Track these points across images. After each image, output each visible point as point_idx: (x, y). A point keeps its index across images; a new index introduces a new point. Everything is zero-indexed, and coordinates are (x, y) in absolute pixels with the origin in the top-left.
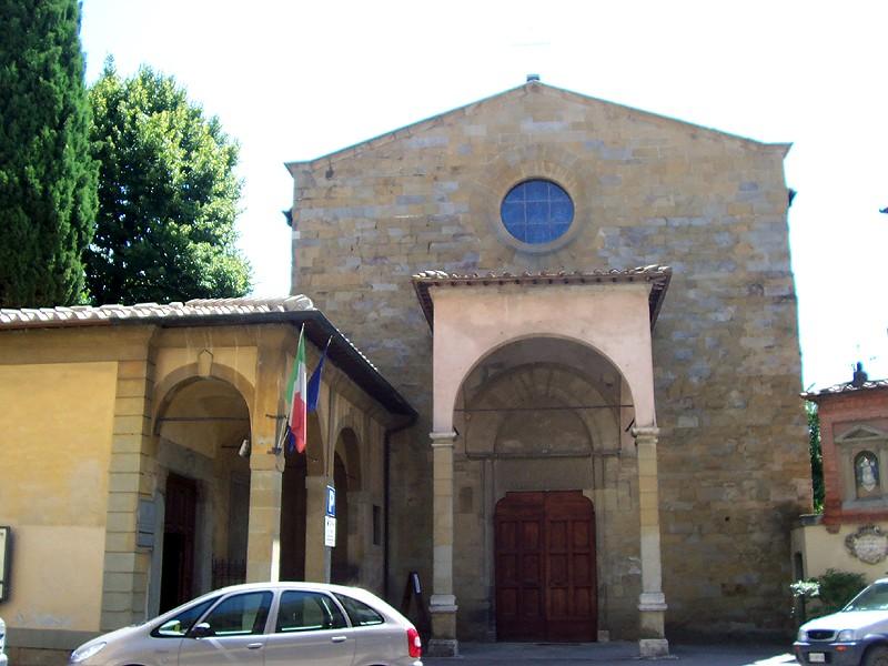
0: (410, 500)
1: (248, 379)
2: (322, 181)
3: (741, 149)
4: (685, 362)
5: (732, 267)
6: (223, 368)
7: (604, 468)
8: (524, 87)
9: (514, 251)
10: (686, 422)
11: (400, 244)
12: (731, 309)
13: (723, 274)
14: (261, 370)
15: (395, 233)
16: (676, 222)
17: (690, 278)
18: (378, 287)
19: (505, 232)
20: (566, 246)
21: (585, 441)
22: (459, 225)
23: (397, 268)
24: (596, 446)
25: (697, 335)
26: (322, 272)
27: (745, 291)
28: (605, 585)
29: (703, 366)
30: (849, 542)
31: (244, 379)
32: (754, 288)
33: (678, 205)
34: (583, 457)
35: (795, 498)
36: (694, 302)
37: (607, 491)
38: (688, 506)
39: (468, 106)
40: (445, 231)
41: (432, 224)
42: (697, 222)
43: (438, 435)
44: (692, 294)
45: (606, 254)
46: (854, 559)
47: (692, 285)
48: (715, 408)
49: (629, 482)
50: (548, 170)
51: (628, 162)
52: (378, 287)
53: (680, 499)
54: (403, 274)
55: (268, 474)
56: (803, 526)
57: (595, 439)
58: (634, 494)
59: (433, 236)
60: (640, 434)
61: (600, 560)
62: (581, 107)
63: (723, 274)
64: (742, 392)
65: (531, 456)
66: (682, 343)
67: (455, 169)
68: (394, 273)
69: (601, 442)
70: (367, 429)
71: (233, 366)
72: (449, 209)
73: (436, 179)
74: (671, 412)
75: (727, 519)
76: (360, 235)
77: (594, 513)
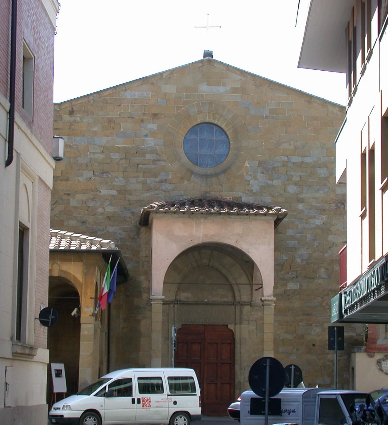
0: (123, 328)
1: (78, 278)
2: (66, 118)
3: (338, 113)
4: (295, 249)
5: (326, 190)
6: (65, 272)
7: (241, 311)
8: (201, 61)
9: (192, 173)
10: (292, 286)
11: (118, 164)
12: (324, 217)
13: (320, 194)
14: (85, 274)
15: (116, 156)
16: (295, 159)
17: (300, 196)
18: (104, 192)
19: (185, 159)
20: (224, 171)
21: (230, 295)
22: (157, 154)
23: (116, 180)
24: (238, 299)
25: (302, 232)
26: (67, 180)
27: (333, 206)
28: (239, 382)
29: (303, 252)
30: (379, 362)
31: (74, 276)
32: (339, 204)
33: (296, 148)
34: (229, 305)
35: (354, 335)
36: (302, 211)
37: (243, 326)
38: (289, 337)
39: (165, 72)
40: (148, 157)
41: (139, 152)
42: (308, 160)
43: (155, 297)
44: (300, 206)
45: (249, 178)
46: (381, 372)
47: (300, 200)
48: (310, 278)
49: (256, 321)
50: (214, 118)
51: (266, 117)
52: (104, 192)
53: (286, 332)
54: (121, 184)
55: (89, 326)
56: (355, 352)
57: (237, 294)
58: (260, 329)
59: (138, 159)
60: (265, 300)
61: (237, 367)
62: (239, 77)
63: (320, 194)
64: (327, 269)
65: (197, 303)
66: (292, 237)
67: (155, 115)
68: (114, 183)
69: (240, 297)
70: (104, 286)
71: (70, 272)
72: (150, 142)
73: (142, 121)
74: (283, 279)
75: (314, 345)
76: (92, 156)
77: (234, 339)
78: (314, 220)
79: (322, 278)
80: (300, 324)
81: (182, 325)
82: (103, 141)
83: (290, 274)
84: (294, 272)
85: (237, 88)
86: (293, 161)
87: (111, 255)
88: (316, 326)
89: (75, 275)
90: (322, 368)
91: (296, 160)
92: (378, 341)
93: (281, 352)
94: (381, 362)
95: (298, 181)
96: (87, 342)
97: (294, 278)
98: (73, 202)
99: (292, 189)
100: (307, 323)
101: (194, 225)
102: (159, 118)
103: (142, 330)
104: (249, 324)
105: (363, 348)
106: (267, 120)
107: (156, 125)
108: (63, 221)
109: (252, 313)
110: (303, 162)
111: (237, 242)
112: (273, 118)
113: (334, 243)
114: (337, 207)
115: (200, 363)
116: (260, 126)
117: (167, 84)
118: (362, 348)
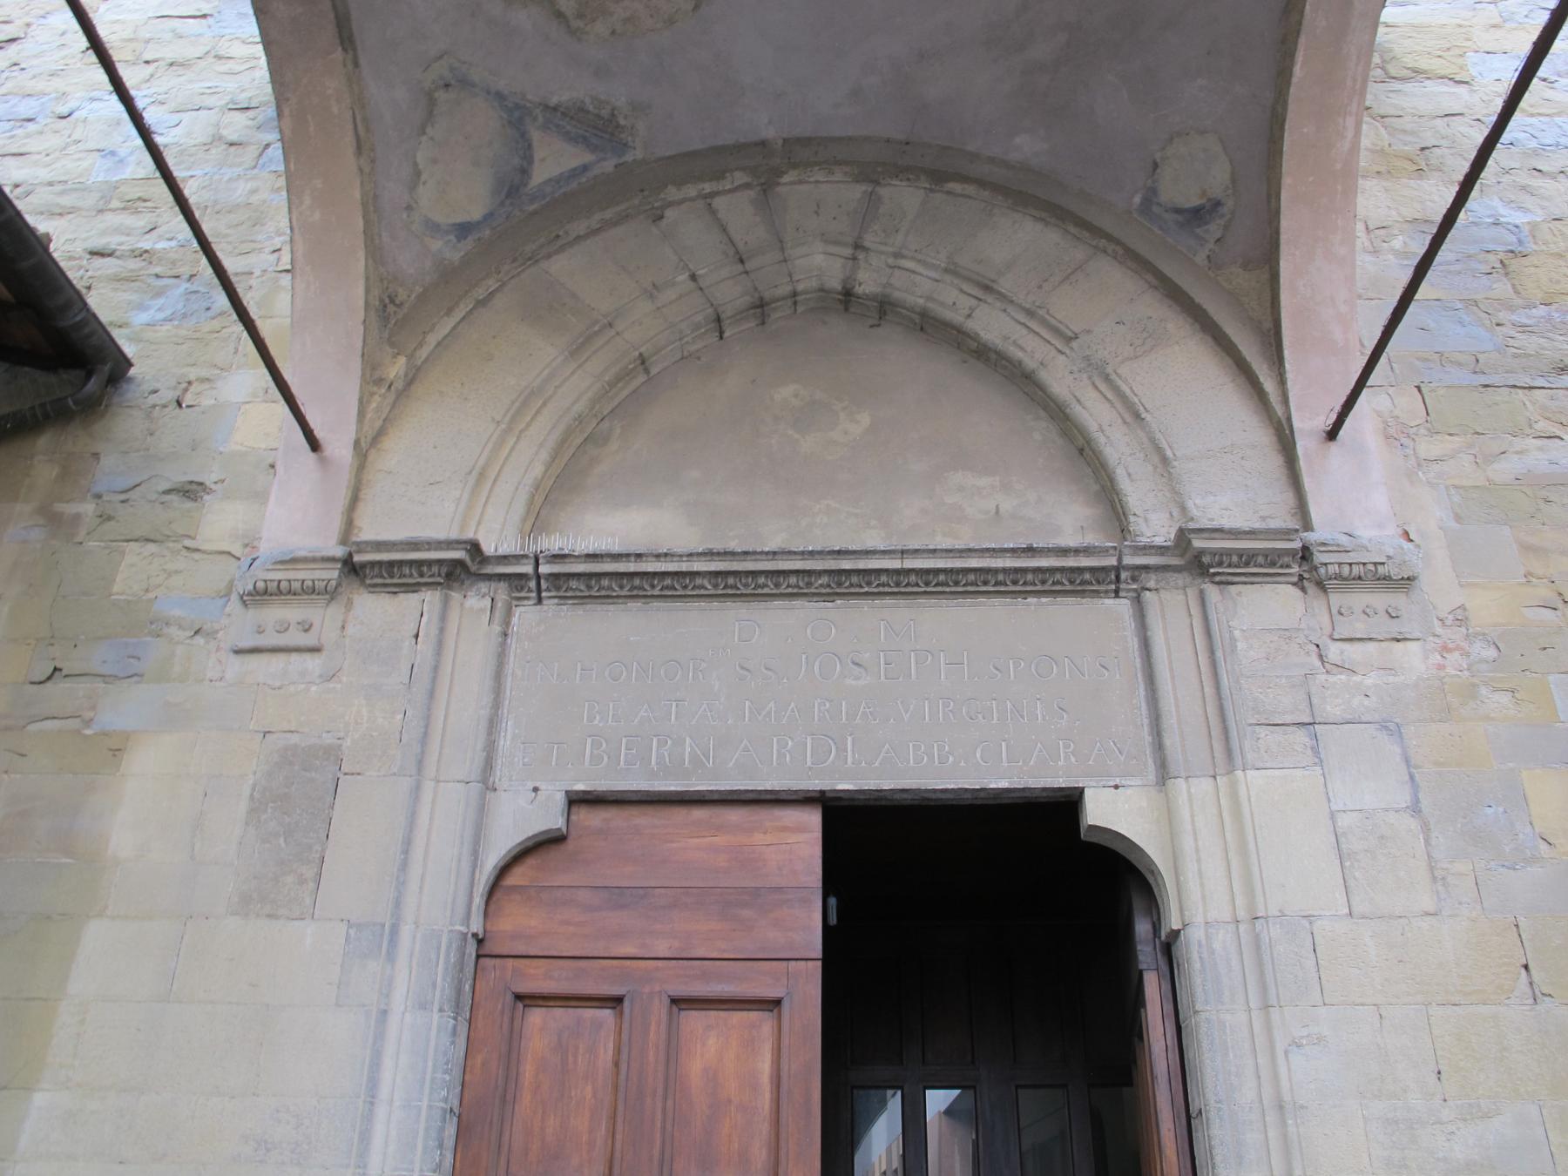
49: (1391, 728)
109: (1334, 651)
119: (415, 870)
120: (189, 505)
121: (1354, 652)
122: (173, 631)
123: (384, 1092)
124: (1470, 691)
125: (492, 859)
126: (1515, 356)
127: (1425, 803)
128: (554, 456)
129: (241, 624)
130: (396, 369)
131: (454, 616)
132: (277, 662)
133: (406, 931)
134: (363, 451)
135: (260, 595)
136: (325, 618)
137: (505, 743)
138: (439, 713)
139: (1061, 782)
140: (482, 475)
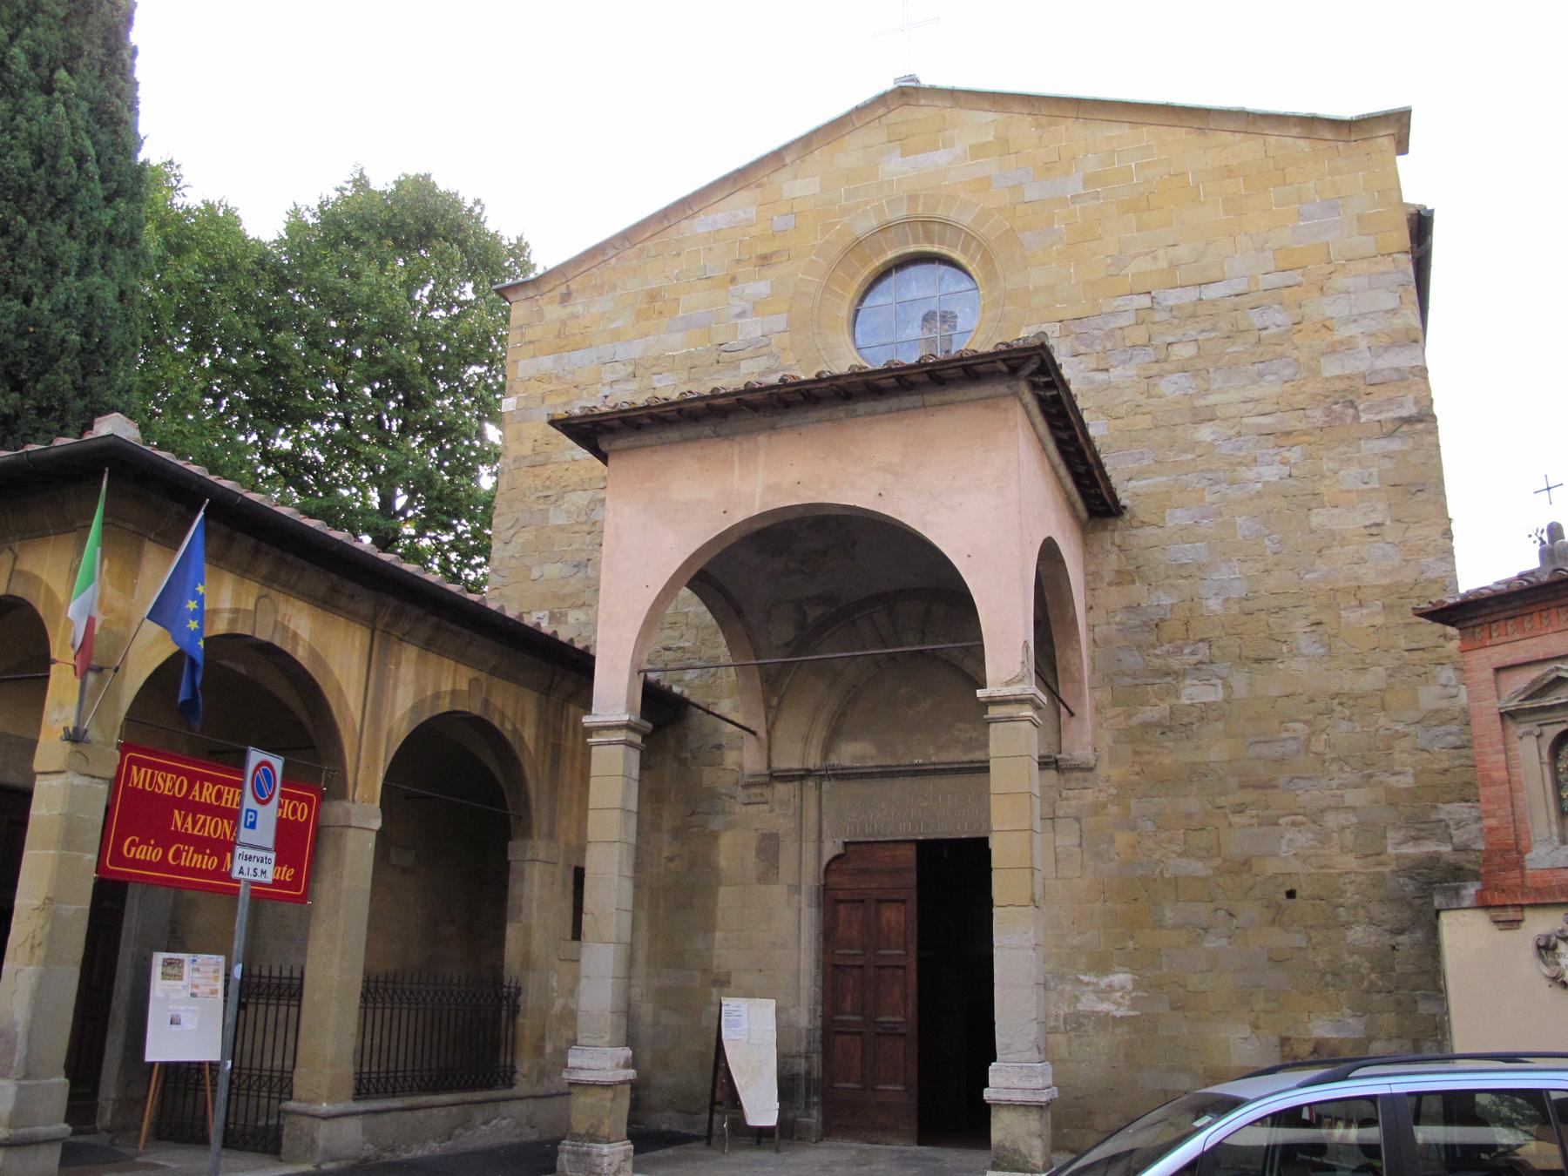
0: (671, 859)
16: (1172, 298)
27: (1318, 416)
29: (1231, 577)
35: (1446, 848)
44: (1205, 433)
47: (1205, 416)
49: (1078, 819)
53: (1184, 854)
72: (753, 328)
73: (733, 280)
78: (1256, 469)
79: (1303, 656)
80: (1235, 819)
81: (846, 844)
82: (634, 349)
83: (1187, 651)
84: (1201, 644)
85: (984, 145)
86: (1170, 303)
87: (107, 469)
88: (1294, 824)
89: (51, 585)
90: (1329, 978)
91: (1177, 298)
92: (1527, 856)
93: (1170, 922)
94: (1555, 947)
95: (1192, 358)
96: (39, 852)
97: (1201, 662)
98: (557, 518)
99: (1171, 387)
100: (1258, 816)
101: (736, 459)
102: (775, 264)
103: (723, 863)
104: (1054, 831)
105: (1465, 888)
106: (1078, 206)
107: (769, 282)
108: (529, 568)
109: (1064, 793)
110: (1200, 299)
111: (882, 492)
112: (1096, 196)
113: (1332, 532)
114: (1333, 415)
115: (903, 967)
116: (1056, 226)
117: (795, 178)
118: (1464, 892)
119: (803, 869)
120: (719, 752)
121: (1071, 793)
122: (724, 797)
123: (802, 929)
124: (1105, 806)
125: (824, 863)
126: (1151, 670)
127: (1084, 845)
128: (829, 726)
129: (742, 794)
130: (775, 701)
131: (805, 788)
132: (756, 807)
133: (803, 886)
134: (769, 733)
135: (747, 786)
136: (767, 792)
137: (825, 827)
138: (804, 821)
139: (982, 835)
140: (807, 738)
